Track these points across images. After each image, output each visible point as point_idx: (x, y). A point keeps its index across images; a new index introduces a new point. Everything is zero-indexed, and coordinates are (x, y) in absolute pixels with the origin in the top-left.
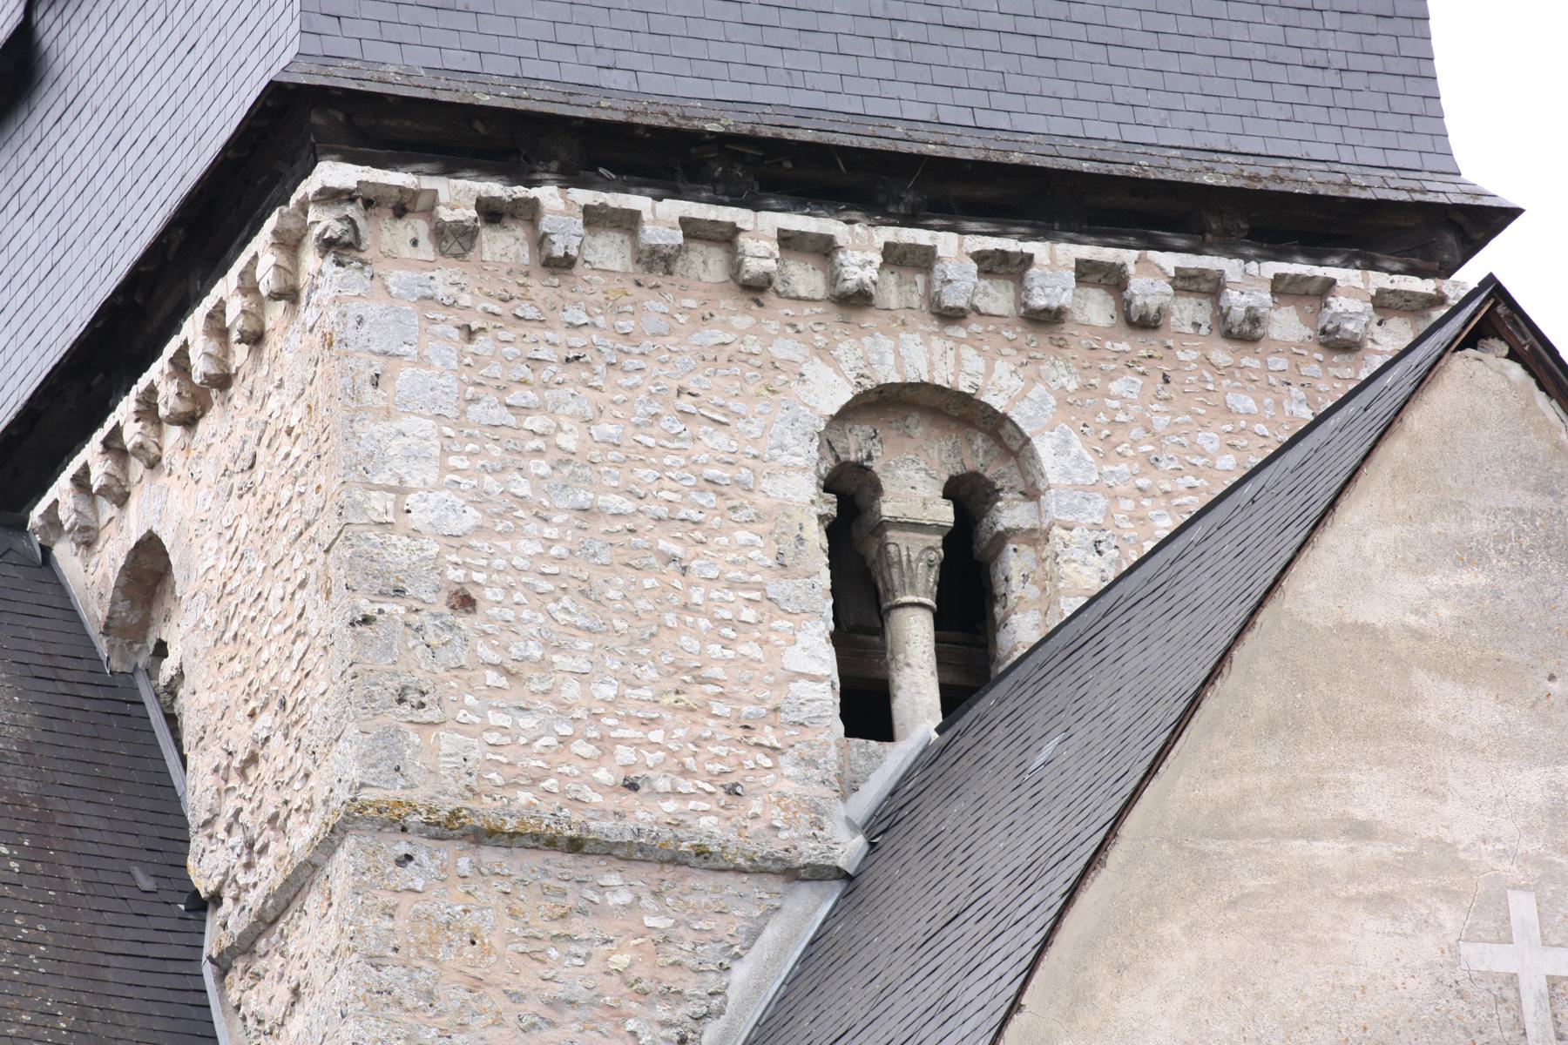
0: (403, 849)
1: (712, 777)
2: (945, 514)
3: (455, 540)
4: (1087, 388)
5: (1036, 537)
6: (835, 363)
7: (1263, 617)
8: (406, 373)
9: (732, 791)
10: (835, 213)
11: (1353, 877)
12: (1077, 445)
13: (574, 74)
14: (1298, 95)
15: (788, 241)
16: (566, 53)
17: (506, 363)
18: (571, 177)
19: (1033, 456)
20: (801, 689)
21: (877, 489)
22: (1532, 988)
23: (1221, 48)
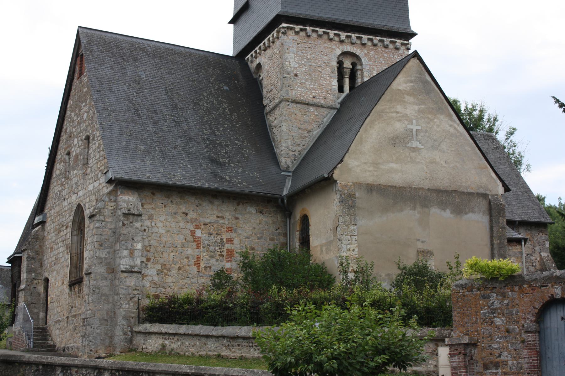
0: (288, 104)
1: (323, 97)
2: (351, 67)
3: (295, 68)
4: (368, 53)
5: (362, 70)
6: (339, 49)
7: (389, 88)
8: (291, 48)
9: (325, 98)
10: (340, 31)
11: (396, 118)
12: (366, 60)
13: (311, 14)
14: (393, 19)
15: (335, 34)
16: (311, 11)
17: (302, 47)
18: (310, 26)
19: (361, 60)
20: (334, 87)
21: (343, 63)
22: (414, 130)
23: (385, 13)
